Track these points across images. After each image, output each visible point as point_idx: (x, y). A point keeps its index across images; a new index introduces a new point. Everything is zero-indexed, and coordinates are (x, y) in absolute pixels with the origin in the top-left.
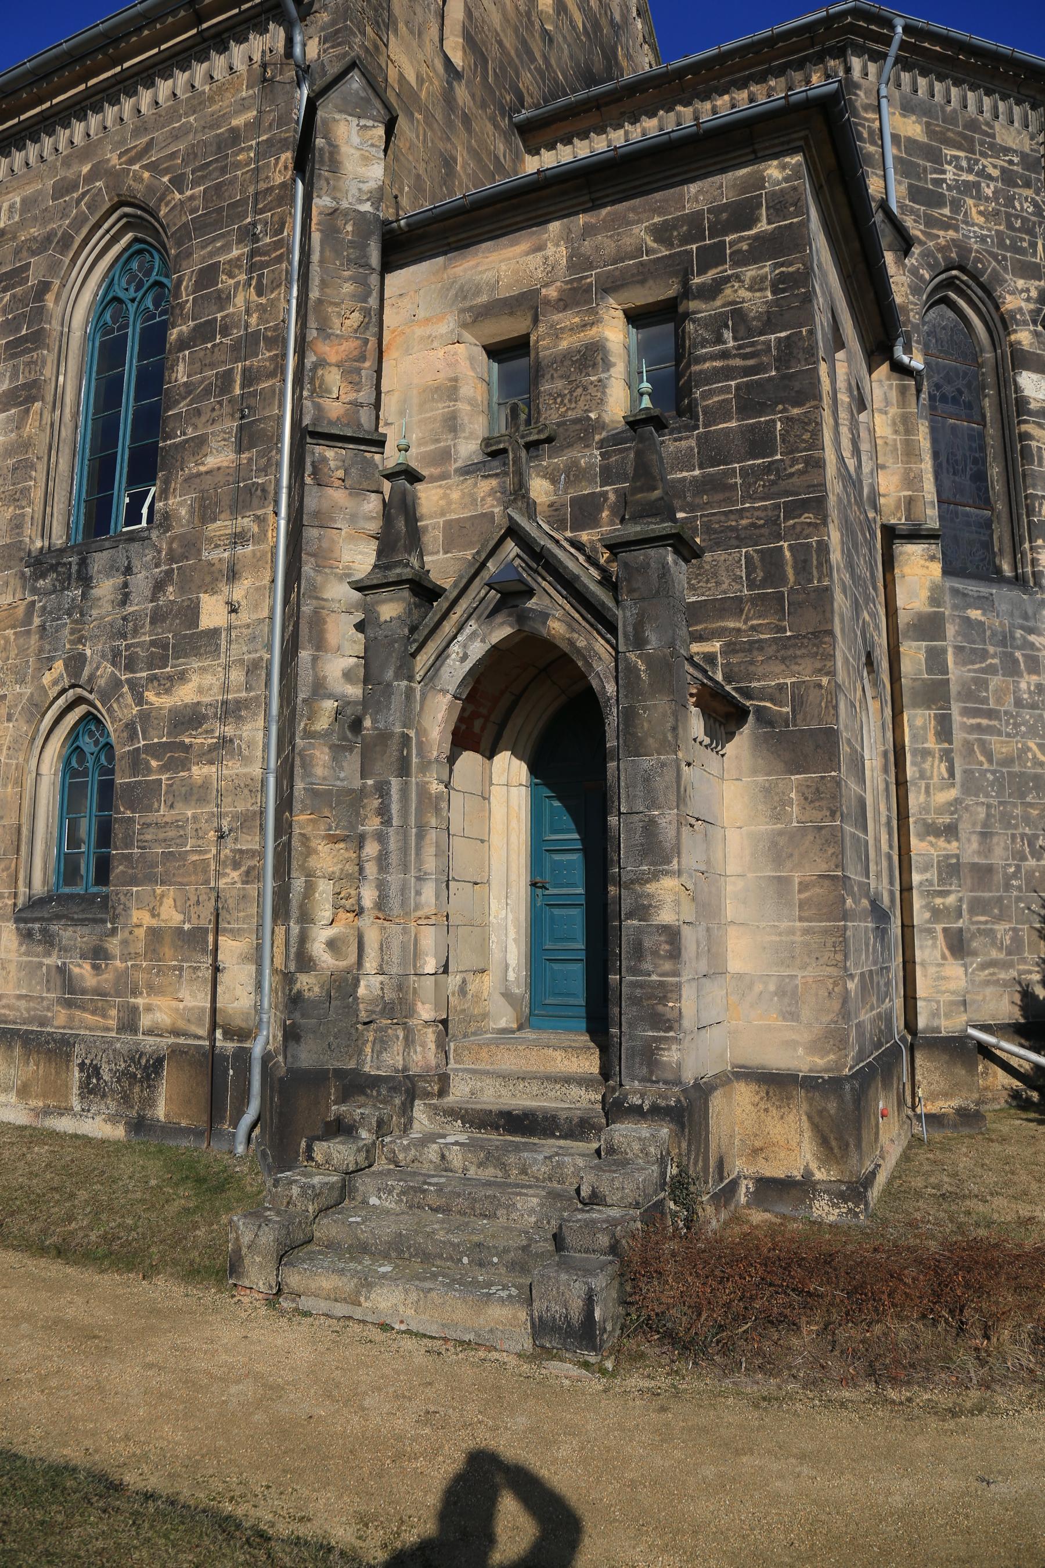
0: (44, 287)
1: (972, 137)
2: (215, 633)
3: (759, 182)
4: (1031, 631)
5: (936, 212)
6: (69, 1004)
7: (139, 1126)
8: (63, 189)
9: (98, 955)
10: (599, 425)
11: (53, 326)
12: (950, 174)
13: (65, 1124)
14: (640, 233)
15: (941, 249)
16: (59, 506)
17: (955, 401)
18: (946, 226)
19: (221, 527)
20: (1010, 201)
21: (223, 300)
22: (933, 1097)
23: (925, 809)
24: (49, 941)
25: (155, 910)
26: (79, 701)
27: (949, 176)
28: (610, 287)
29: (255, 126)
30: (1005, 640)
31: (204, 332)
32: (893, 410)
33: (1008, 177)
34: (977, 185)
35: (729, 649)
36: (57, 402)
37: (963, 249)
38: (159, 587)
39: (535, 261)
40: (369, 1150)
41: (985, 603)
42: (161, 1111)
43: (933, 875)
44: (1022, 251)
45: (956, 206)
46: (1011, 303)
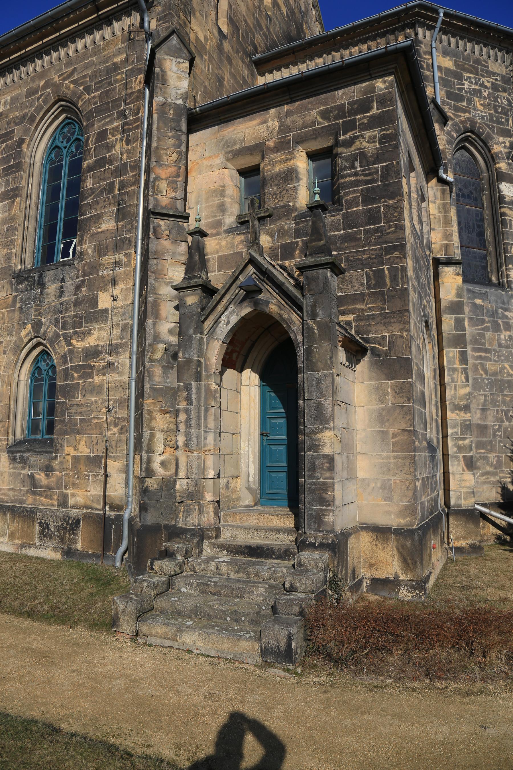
0: (22, 141)
1: (477, 67)
2: (105, 311)
3: (373, 89)
4: (506, 310)
5: (460, 104)
6: (34, 493)
7: (68, 553)
8: (31, 93)
9: (48, 469)
10: (294, 209)
11: (26, 160)
12: (466, 85)
13: (32, 552)
14: (314, 114)
15: (462, 122)
16: (29, 249)
17: (469, 197)
18: (464, 111)
19: (108, 259)
20: (496, 99)
21: (109, 147)
22: (458, 538)
23: (454, 397)
24: (24, 462)
25: (76, 447)
26: (39, 344)
27: (466, 86)
28: (299, 141)
29: (125, 62)
30: (493, 314)
31: (100, 163)
32: (439, 202)
33: (495, 87)
34: (479, 91)
35: (358, 319)
36: (29, 197)
37: (473, 122)
38: (78, 288)
39: (262, 128)
40: (181, 565)
41: (484, 296)
42: (79, 546)
43: (458, 430)
44: (501, 123)
45: (469, 101)
46: (496, 149)
